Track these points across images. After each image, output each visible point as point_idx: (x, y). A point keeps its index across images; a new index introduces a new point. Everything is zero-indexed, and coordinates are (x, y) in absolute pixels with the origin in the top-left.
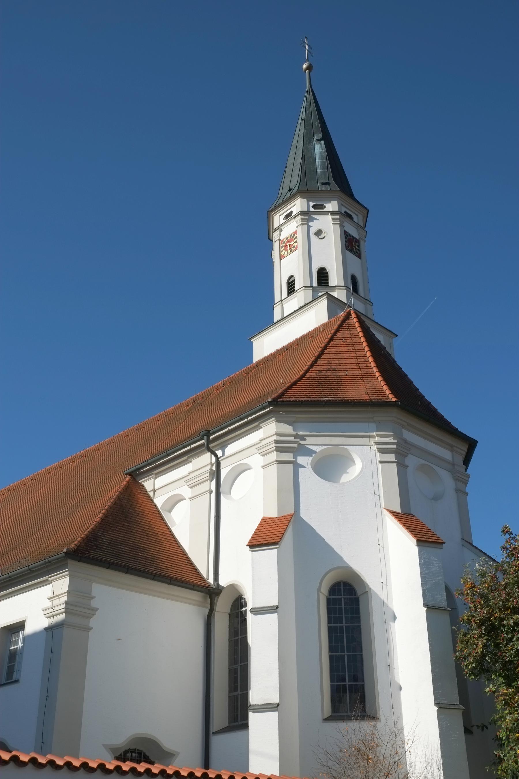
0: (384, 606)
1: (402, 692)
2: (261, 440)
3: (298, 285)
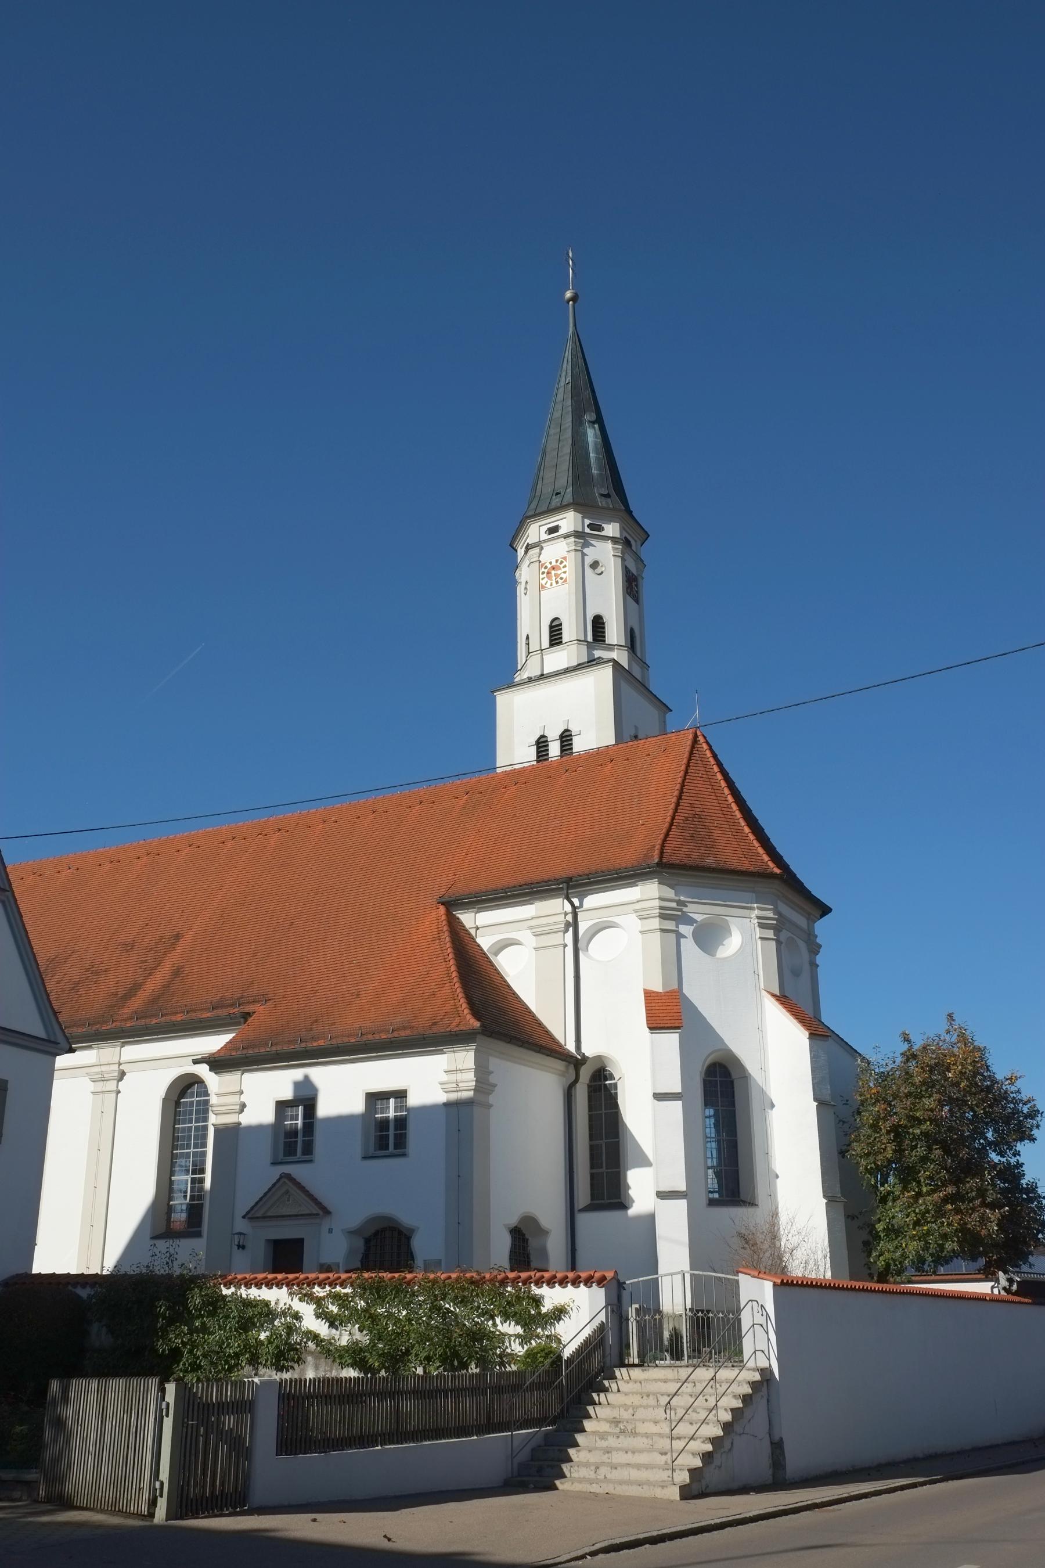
0: (763, 1093)
1: (778, 1181)
3: (566, 637)
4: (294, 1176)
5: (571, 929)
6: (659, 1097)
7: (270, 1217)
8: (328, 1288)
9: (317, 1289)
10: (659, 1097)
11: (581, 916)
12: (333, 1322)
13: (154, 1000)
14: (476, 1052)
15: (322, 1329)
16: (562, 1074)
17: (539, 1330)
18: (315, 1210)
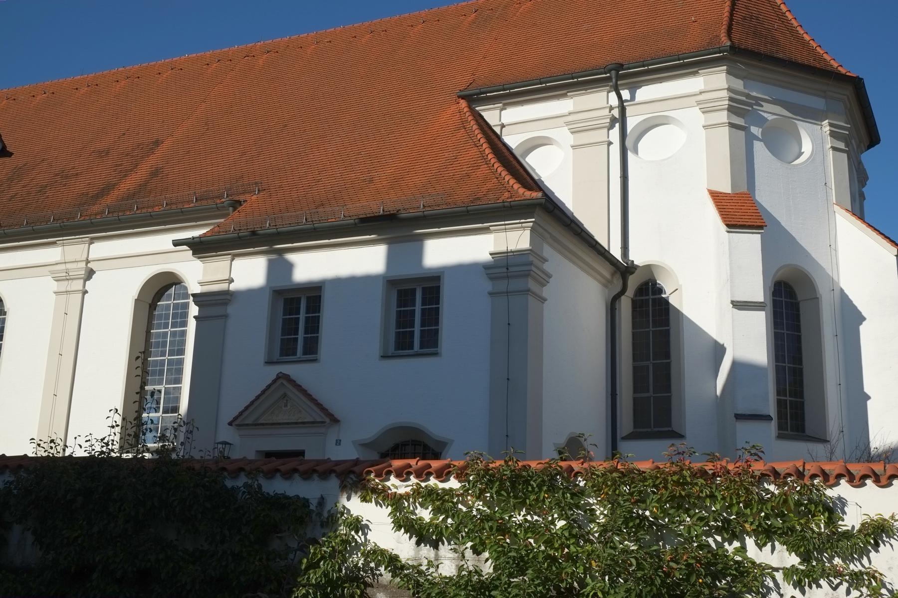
2: (701, 93)
4: (293, 377)
5: (617, 125)
6: (739, 305)
7: (263, 424)
8: (413, 480)
9: (393, 481)
10: (739, 305)
11: (629, 111)
12: (423, 535)
13: (131, 196)
14: (533, 230)
15: (403, 547)
16: (606, 284)
17: (837, 561)
18: (319, 416)
